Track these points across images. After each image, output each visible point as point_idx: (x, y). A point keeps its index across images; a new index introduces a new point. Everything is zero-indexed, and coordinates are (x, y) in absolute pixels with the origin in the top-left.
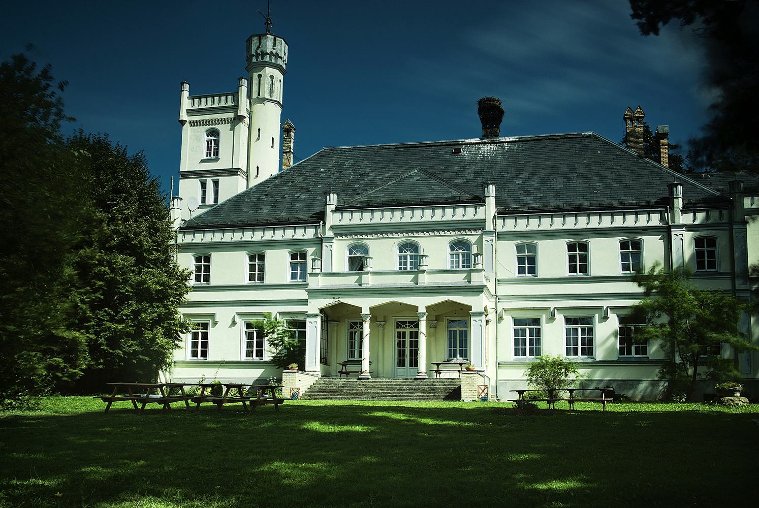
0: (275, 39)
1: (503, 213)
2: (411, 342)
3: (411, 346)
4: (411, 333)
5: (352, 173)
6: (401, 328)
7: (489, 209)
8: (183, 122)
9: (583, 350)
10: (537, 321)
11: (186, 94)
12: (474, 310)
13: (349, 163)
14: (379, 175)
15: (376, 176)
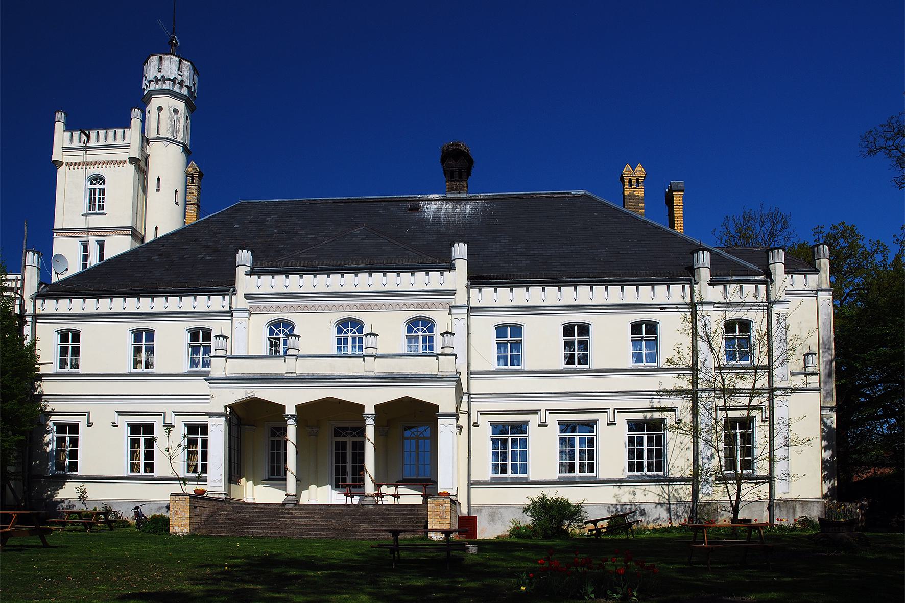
0: (180, 62)
1: (477, 279)
2: (354, 456)
3: (354, 461)
4: (354, 443)
5: (276, 231)
6: (339, 436)
7: (458, 277)
8: (59, 164)
9: (582, 466)
10: (590, 425)
11: (59, 126)
12: (441, 411)
13: (272, 219)
14: (311, 234)
15: (307, 234)
